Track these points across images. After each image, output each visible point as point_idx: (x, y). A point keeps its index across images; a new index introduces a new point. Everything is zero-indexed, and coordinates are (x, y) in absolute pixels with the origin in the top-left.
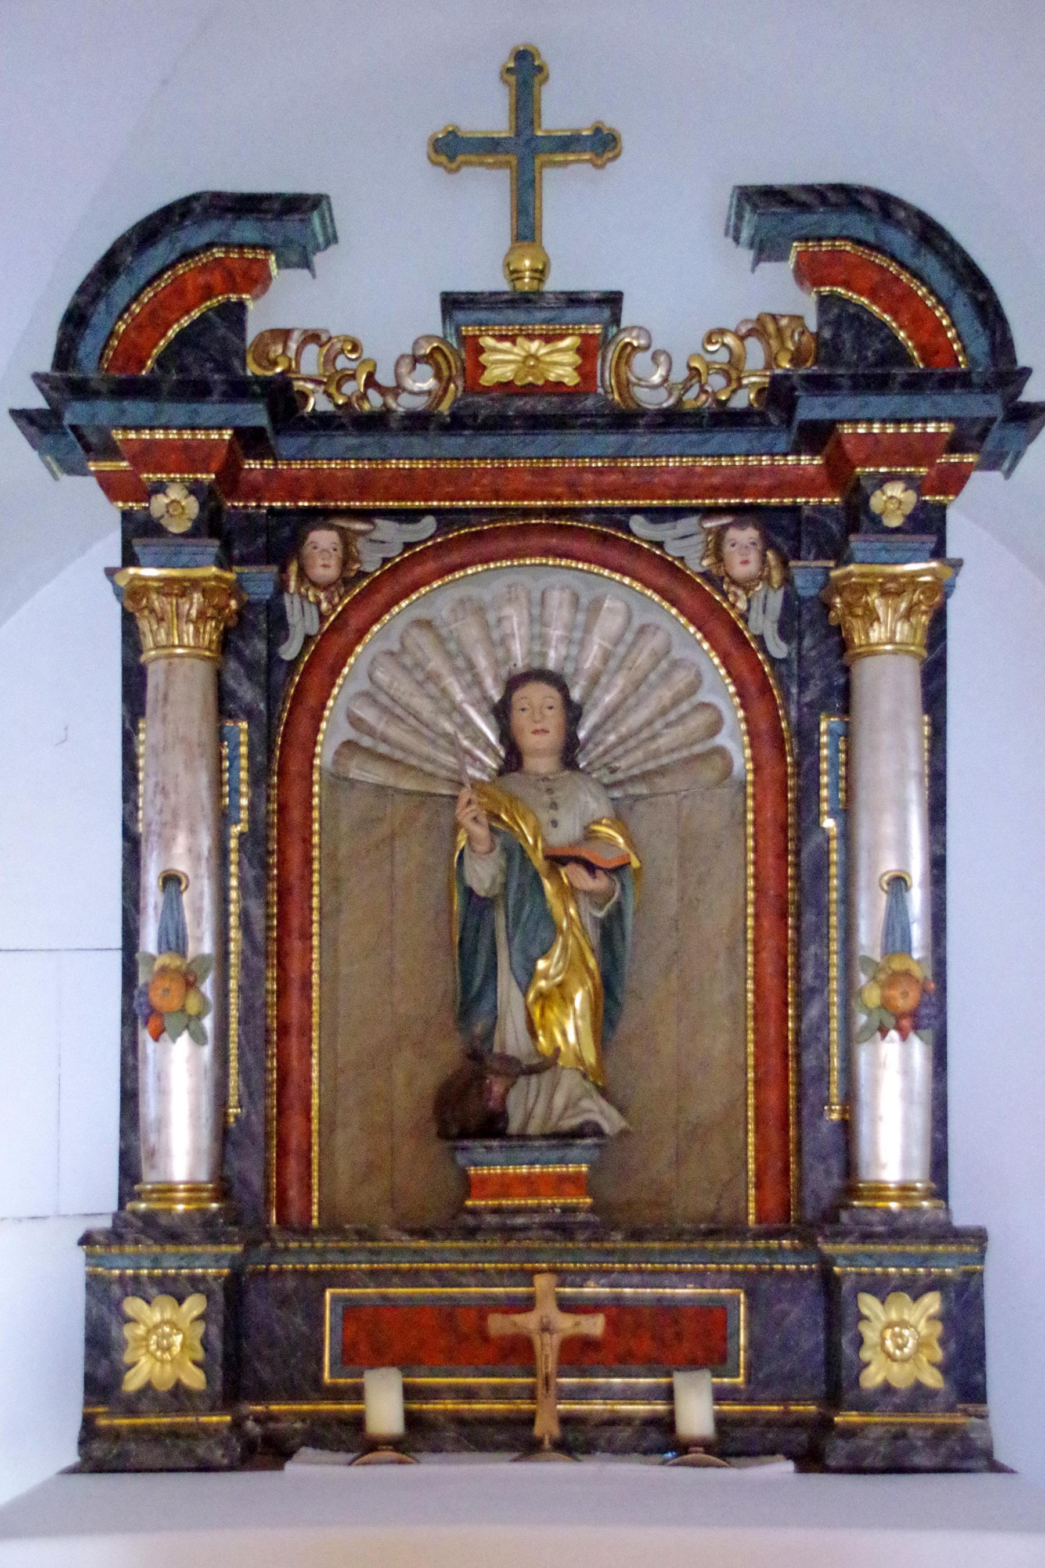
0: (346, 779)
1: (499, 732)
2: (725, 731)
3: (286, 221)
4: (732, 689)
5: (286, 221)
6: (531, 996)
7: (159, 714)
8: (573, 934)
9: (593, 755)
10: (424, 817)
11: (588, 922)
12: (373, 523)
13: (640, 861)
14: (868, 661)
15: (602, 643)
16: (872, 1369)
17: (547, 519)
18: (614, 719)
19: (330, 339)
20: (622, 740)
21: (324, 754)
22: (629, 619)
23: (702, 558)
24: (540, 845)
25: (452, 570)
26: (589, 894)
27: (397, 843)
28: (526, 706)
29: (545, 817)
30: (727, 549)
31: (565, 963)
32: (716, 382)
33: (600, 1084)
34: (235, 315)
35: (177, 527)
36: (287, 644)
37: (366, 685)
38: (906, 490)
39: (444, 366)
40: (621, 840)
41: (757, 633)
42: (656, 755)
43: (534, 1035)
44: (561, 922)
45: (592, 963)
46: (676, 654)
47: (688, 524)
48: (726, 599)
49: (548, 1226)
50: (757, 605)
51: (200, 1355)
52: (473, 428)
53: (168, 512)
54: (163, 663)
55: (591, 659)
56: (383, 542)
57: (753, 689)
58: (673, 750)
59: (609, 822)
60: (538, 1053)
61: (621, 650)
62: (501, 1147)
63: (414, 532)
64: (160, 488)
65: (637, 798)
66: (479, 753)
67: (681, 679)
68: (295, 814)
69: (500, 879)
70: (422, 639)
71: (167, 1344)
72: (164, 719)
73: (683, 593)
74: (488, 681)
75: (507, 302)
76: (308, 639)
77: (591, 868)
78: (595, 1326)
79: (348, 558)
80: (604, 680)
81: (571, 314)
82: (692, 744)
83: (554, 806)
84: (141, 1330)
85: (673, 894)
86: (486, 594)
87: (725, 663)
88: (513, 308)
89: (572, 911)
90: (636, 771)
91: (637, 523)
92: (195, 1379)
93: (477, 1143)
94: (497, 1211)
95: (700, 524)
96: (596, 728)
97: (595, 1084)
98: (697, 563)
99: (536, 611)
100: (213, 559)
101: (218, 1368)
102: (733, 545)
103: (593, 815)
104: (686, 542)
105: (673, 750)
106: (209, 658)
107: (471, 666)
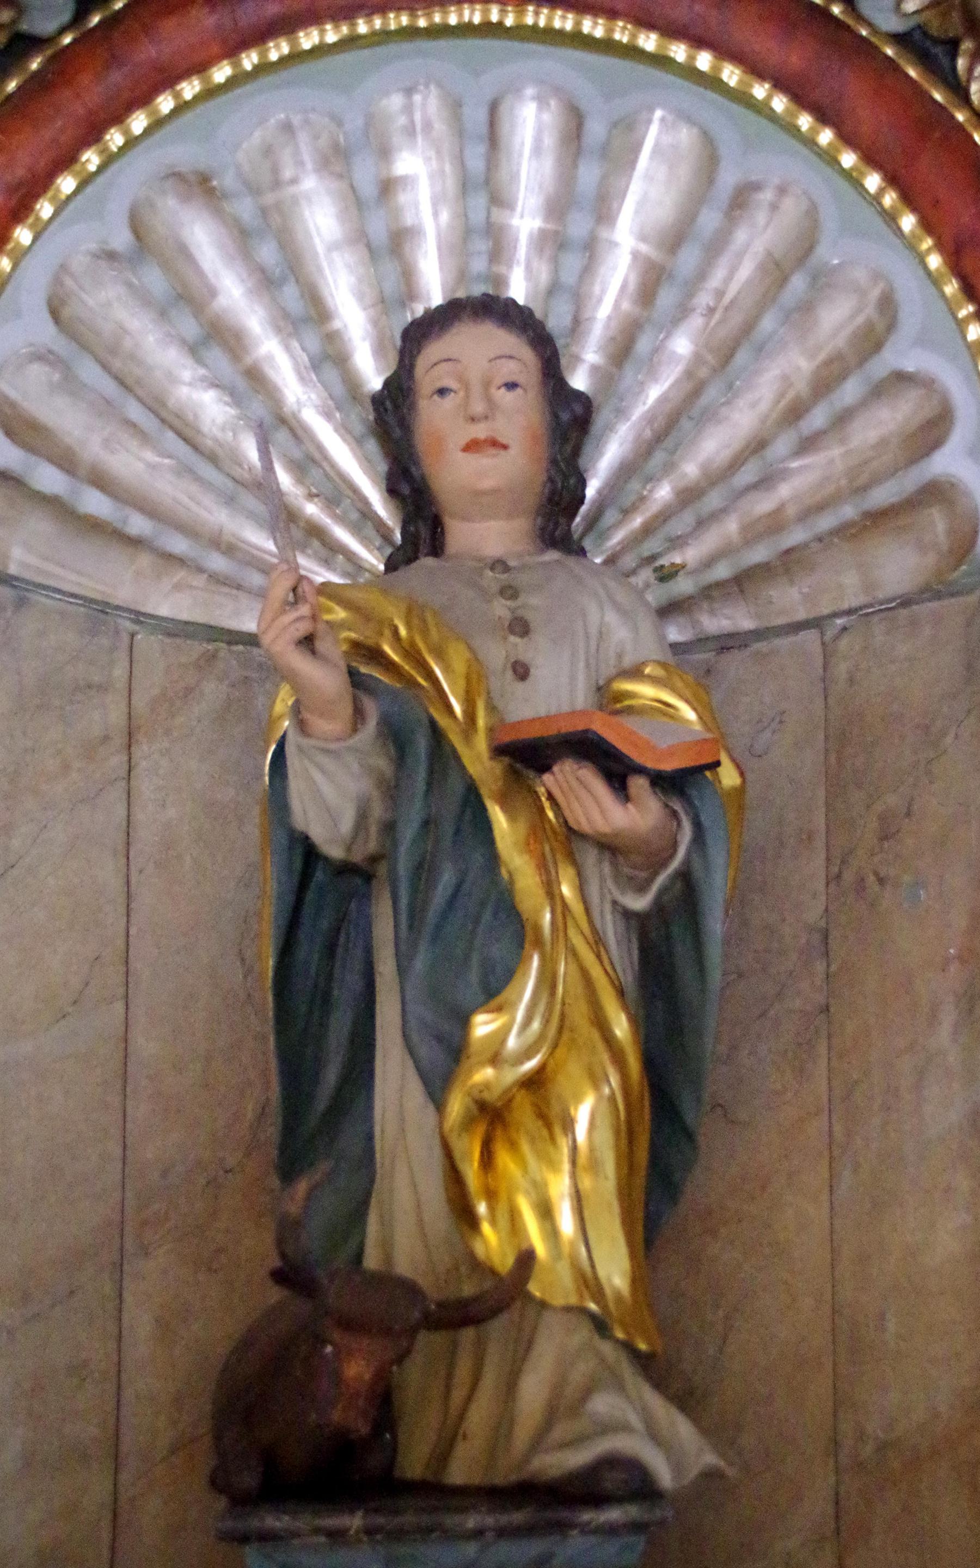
1: (383, 467)
2: (959, 438)
6: (456, 1105)
8: (573, 953)
9: (618, 537)
10: (213, 691)
11: (611, 928)
13: (742, 774)
18: (669, 443)
20: (688, 496)
22: (709, 161)
24: (481, 722)
26: (609, 847)
27: (142, 749)
29: (496, 654)
31: (546, 1022)
33: (642, 1346)
37: (45, 332)
40: (690, 714)
42: (774, 523)
43: (466, 1217)
44: (538, 912)
45: (621, 1027)
46: (829, 253)
58: (821, 507)
59: (659, 672)
60: (478, 1267)
61: (688, 258)
62: (370, 1532)
65: (728, 643)
66: (342, 534)
67: (837, 319)
69: (378, 811)
73: (854, 88)
77: (617, 771)
80: (643, 345)
82: (864, 489)
83: (520, 627)
85: (815, 865)
87: (956, 265)
89: (566, 890)
90: (722, 571)
93: (303, 1522)
96: (627, 471)
97: (628, 1347)
99: (476, 158)
103: (620, 656)
105: (821, 507)
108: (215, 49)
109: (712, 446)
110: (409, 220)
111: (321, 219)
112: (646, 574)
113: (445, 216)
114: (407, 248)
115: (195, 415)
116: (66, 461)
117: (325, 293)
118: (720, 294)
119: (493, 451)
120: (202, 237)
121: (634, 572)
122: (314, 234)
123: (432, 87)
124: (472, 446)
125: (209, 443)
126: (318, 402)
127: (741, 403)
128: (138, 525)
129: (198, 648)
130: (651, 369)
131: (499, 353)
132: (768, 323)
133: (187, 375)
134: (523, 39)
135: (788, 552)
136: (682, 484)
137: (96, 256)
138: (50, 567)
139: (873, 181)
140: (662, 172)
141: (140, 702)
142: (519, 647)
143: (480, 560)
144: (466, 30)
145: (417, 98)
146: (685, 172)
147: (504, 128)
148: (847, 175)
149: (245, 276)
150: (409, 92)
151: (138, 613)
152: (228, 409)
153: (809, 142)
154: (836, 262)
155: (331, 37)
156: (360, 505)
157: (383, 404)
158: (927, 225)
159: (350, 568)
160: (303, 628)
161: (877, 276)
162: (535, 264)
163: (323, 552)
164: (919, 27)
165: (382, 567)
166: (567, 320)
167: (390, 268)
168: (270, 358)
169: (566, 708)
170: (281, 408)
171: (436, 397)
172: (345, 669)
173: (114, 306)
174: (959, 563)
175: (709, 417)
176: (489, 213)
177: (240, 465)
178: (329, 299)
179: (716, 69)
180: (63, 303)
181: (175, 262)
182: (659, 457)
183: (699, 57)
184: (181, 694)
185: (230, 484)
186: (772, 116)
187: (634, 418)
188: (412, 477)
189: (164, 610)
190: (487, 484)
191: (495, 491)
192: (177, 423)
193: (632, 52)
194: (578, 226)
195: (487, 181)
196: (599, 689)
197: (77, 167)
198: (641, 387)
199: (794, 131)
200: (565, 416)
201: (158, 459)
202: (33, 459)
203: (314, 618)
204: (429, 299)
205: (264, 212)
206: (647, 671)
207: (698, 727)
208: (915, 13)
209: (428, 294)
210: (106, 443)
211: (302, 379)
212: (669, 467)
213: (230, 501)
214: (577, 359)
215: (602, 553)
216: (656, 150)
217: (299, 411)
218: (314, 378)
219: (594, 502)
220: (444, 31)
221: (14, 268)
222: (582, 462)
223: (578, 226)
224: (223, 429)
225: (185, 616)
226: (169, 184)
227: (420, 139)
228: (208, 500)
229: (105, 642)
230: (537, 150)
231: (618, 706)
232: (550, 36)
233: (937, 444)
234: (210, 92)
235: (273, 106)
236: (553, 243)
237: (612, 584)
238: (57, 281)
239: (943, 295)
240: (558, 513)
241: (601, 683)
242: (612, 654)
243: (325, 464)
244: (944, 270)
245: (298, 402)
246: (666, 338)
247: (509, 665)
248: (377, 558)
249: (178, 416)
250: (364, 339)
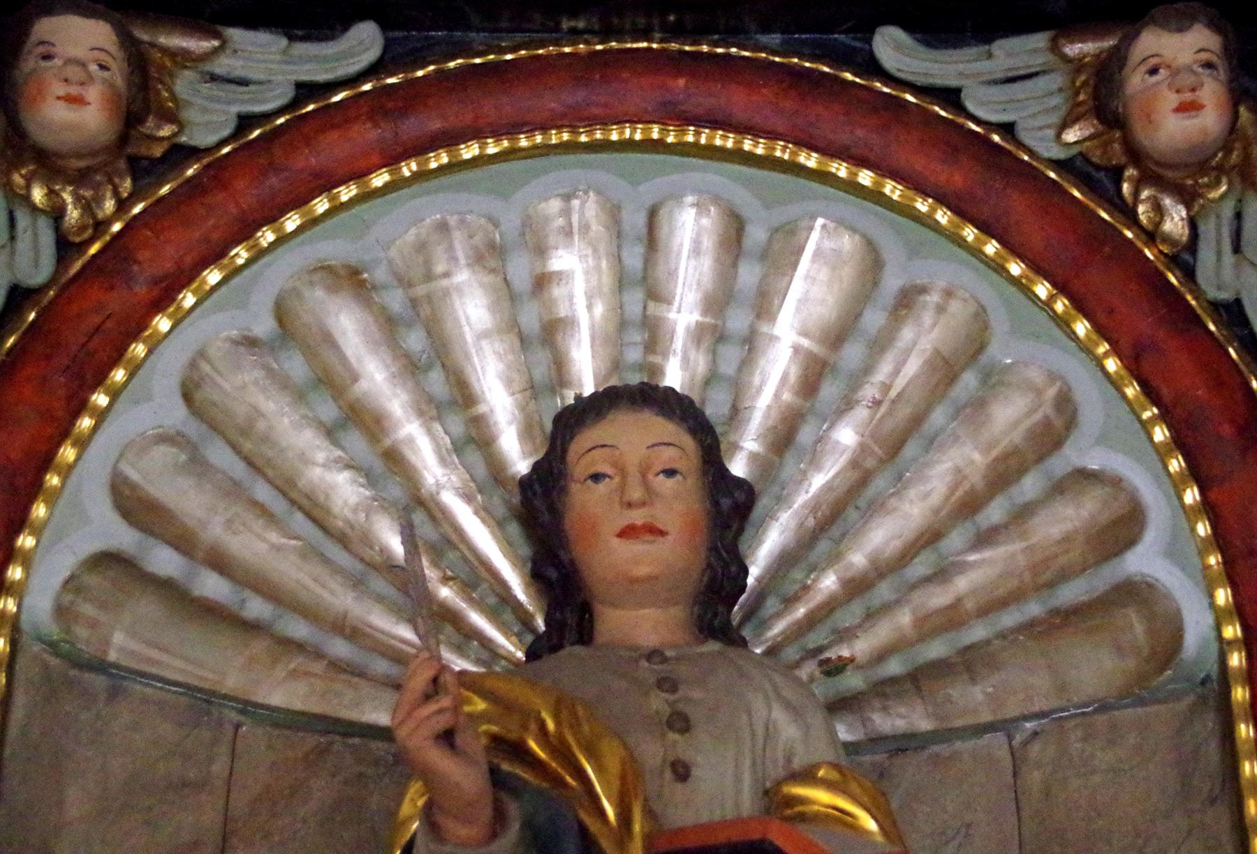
0: (101, 666)
1: (526, 551)
2: (1152, 537)
4: (1160, 434)
10: (322, 790)
12: (216, 35)
15: (806, 343)
17: (661, 41)
18: (835, 531)
20: (856, 587)
22: (873, 263)
23: (1064, 126)
24: (637, 827)
25: (420, 149)
28: (609, 470)
29: (652, 752)
37: (176, 415)
40: (871, 825)
41: (1224, 296)
42: (952, 618)
46: (1001, 351)
50: (1214, 233)
56: (243, 82)
58: (1003, 603)
61: (853, 353)
65: (904, 744)
66: (478, 620)
67: (1010, 416)
73: (1017, 204)
79: (143, 95)
80: (806, 435)
82: (1051, 585)
83: (680, 722)
87: (1134, 367)
90: (894, 667)
95: (1055, 48)
96: (786, 561)
98: (1051, 132)
99: (634, 257)
102: (1153, 71)
103: (789, 760)
104: (1017, 89)
108: (375, 159)
109: (880, 537)
110: (563, 312)
111: (472, 309)
112: (808, 670)
113: (599, 309)
114: (559, 338)
115: (327, 496)
116: (184, 543)
117: (473, 379)
118: (886, 388)
119: (649, 537)
120: (348, 326)
121: (797, 664)
122: (464, 322)
123: (591, 194)
124: (628, 532)
125: (340, 524)
126: (458, 485)
127: (912, 493)
128: (256, 608)
129: (312, 741)
130: (814, 459)
131: (655, 441)
132: (938, 416)
133: (320, 456)
134: (683, 154)
135: (969, 648)
136: (849, 574)
137: (235, 343)
138: (154, 654)
139: (1042, 290)
140: (824, 274)
141: (240, 802)
142: (680, 745)
143: (635, 648)
144: (627, 146)
145: (576, 203)
146: (848, 273)
147: (663, 232)
148: (1015, 281)
149: (389, 361)
150: (567, 198)
151: (247, 703)
152: (362, 490)
153: (975, 252)
154: (1009, 361)
155: (492, 149)
156: (499, 589)
157: (531, 486)
158: (1101, 330)
159: (485, 655)
160: (441, 723)
161: (1052, 377)
162: (692, 354)
163: (456, 638)
164: (1081, 154)
165: (520, 655)
166: (725, 410)
167: (542, 358)
168: (410, 440)
169: (730, 814)
170: (419, 490)
171: (589, 482)
172: (485, 767)
173: (250, 392)
174: (1162, 670)
175: (877, 507)
176: (645, 308)
177: (371, 548)
178: (476, 385)
179: (878, 184)
180: (198, 386)
181: (319, 347)
182: (823, 546)
183: (861, 174)
184: (286, 792)
185: (360, 567)
186: (936, 227)
187: (796, 506)
188: (560, 562)
189: (277, 698)
190: (642, 571)
191: (651, 578)
192: (305, 502)
193: (795, 169)
194: (738, 321)
195: (644, 278)
196: (766, 792)
197: (225, 261)
198: (804, 476)
199: (961, 242)
200: (726, 503)
201: (284, 540)
202: (151, 540)
203: (456, 709)
204: (581, 386)
205: (414, 303)
206: (821, 773)
207: (880, 839)
208: (1076, 143)
209: (580, 380)
210: (229, 523)
211: (443, 461)
212: (834, 558)
213: (357, 584)
214: (735, 447)
215: (762, 643)
216: (818, 254)
217: (438, 493)
218: (456, 460)
219: (754, 589)
220: (606, 146)
221: (147, 355)
222: (743, 547)
223: (738, 321)
224: (355, 510)
225: (298, 705)
226: (317, 277)
227: (576, 238)
228: (335, 584)
229: (206, 734)
230: (696, 251)
231: (788, 812)
232: (711, 152)
233: (1131, 542)
234: (367, 196)
235: (429, 208)
236: (712, 335)
237: (778, 678)
238: (193, 365)
239: (1124, 396)
240: (717, 599)
241: (768, 784)
242: (780, 755)
243: (461, 546)
244: (1123, 372)
245: (437, 484)
246: (829, 428)
247: (668, 764)
248: (514, 645)
249: (308, 497)
250: (510, 423)
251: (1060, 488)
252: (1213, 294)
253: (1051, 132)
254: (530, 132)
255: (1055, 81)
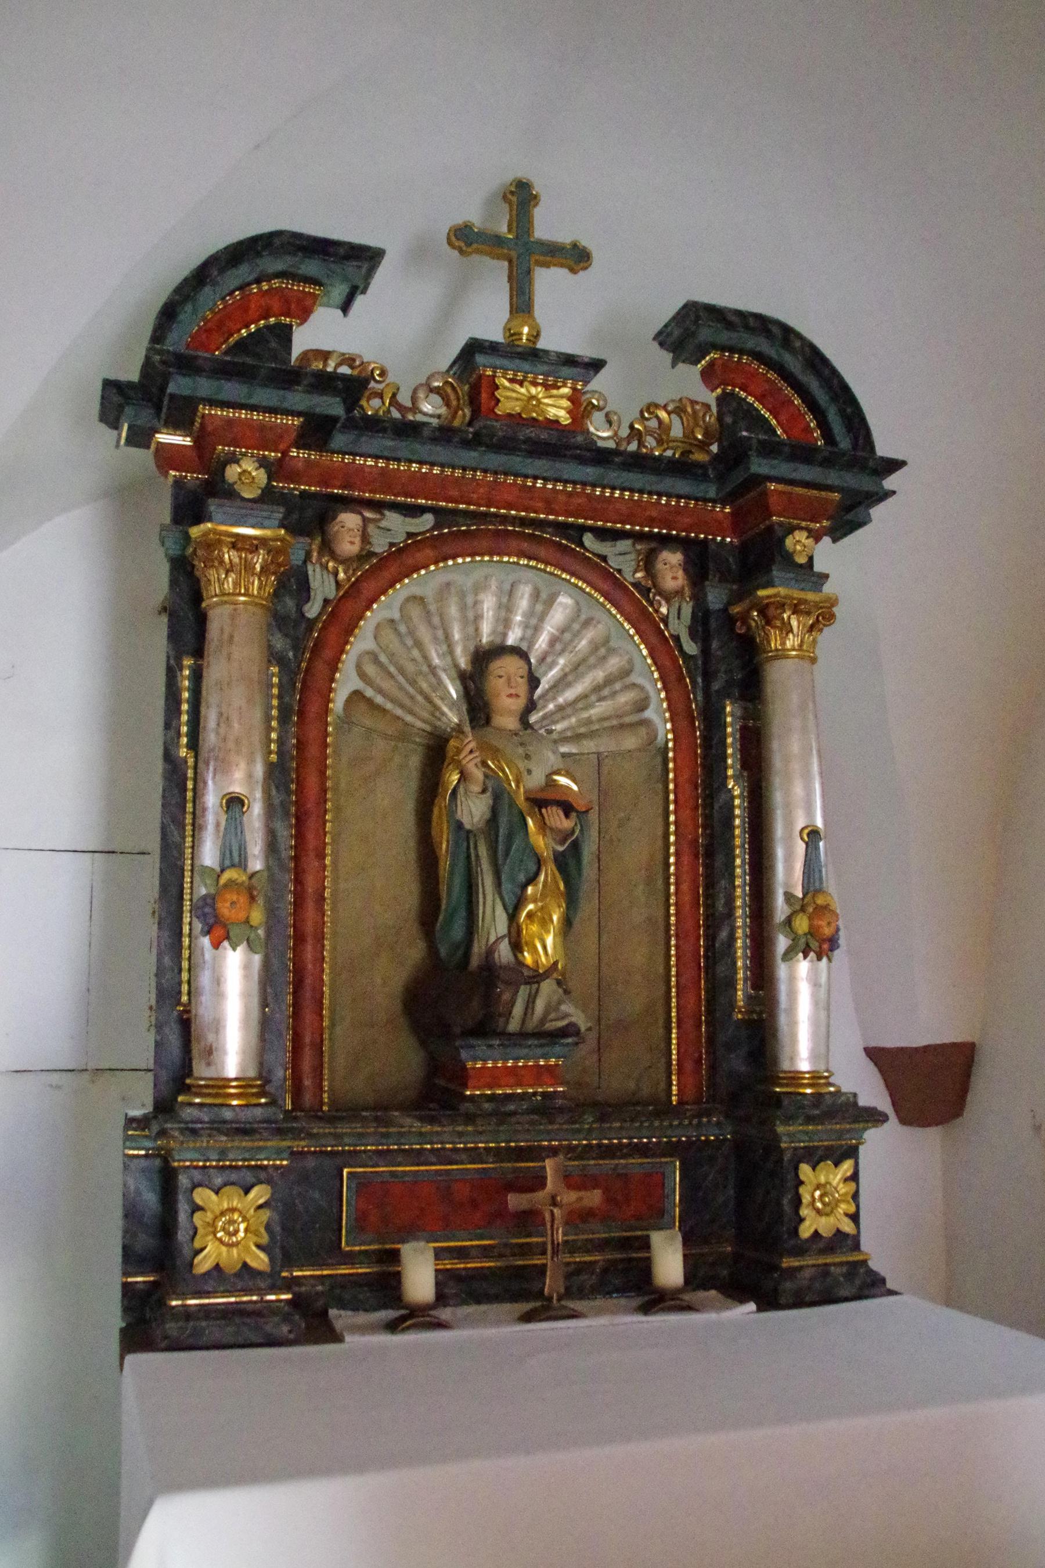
3: (350, 264)
5: (350, 264)
7: (225, 653)
14: (777, 664)
16: (807, 1223)
19: (363, 363)
20: (560, 708)
21: (338, 703)
22: (578, 611)
23: (635, 572)
30: (659, 566)
32: (650, 442)
34: (285, 335)
35: (249, 493)
36: (309, 604)
38: (807, 538)
39: (452, 397)
41: (676, 633)
42: (589, 721)
47: (625, 545)
48: (652, 605)
49: (533, 1111)
51: (265, 1239)
52: (487, 446)
53: (240, 479)
54: (228, 609)
55: (542, 642)
57: (673, 677)
61: (567, 636)
63: (417, 525)
64: (234, 460)
67: (614, 663)
68: (313, 751)
70: (415, 612)
71: (230, 1230)
72: (229, 658)
74: (459, 650)
75: (519, 353)
76: (326, 602)
78: (594, 1198)
80: (549, 660)
81: (566, 371)
83: (527, 757)
84: (209, 1216)
86: (466, 581)
87: (652, 654)
88: (520, 358)
91: (588, 539)
92: (260, 1260)
94: (492, 1098)
95: (634, 545)
98: (633, 574)
99: (505, 600)
100: (277, 523)
101: (277, 1250)
104: (621, 558)
106: (264, 605)
107: (448, 637)
109: (569, 695)
175: (569, 685)
251: (627, 688)
252: (672, 632)
253: (633, 574)
254: (411, 497)
255: (633, 556)
